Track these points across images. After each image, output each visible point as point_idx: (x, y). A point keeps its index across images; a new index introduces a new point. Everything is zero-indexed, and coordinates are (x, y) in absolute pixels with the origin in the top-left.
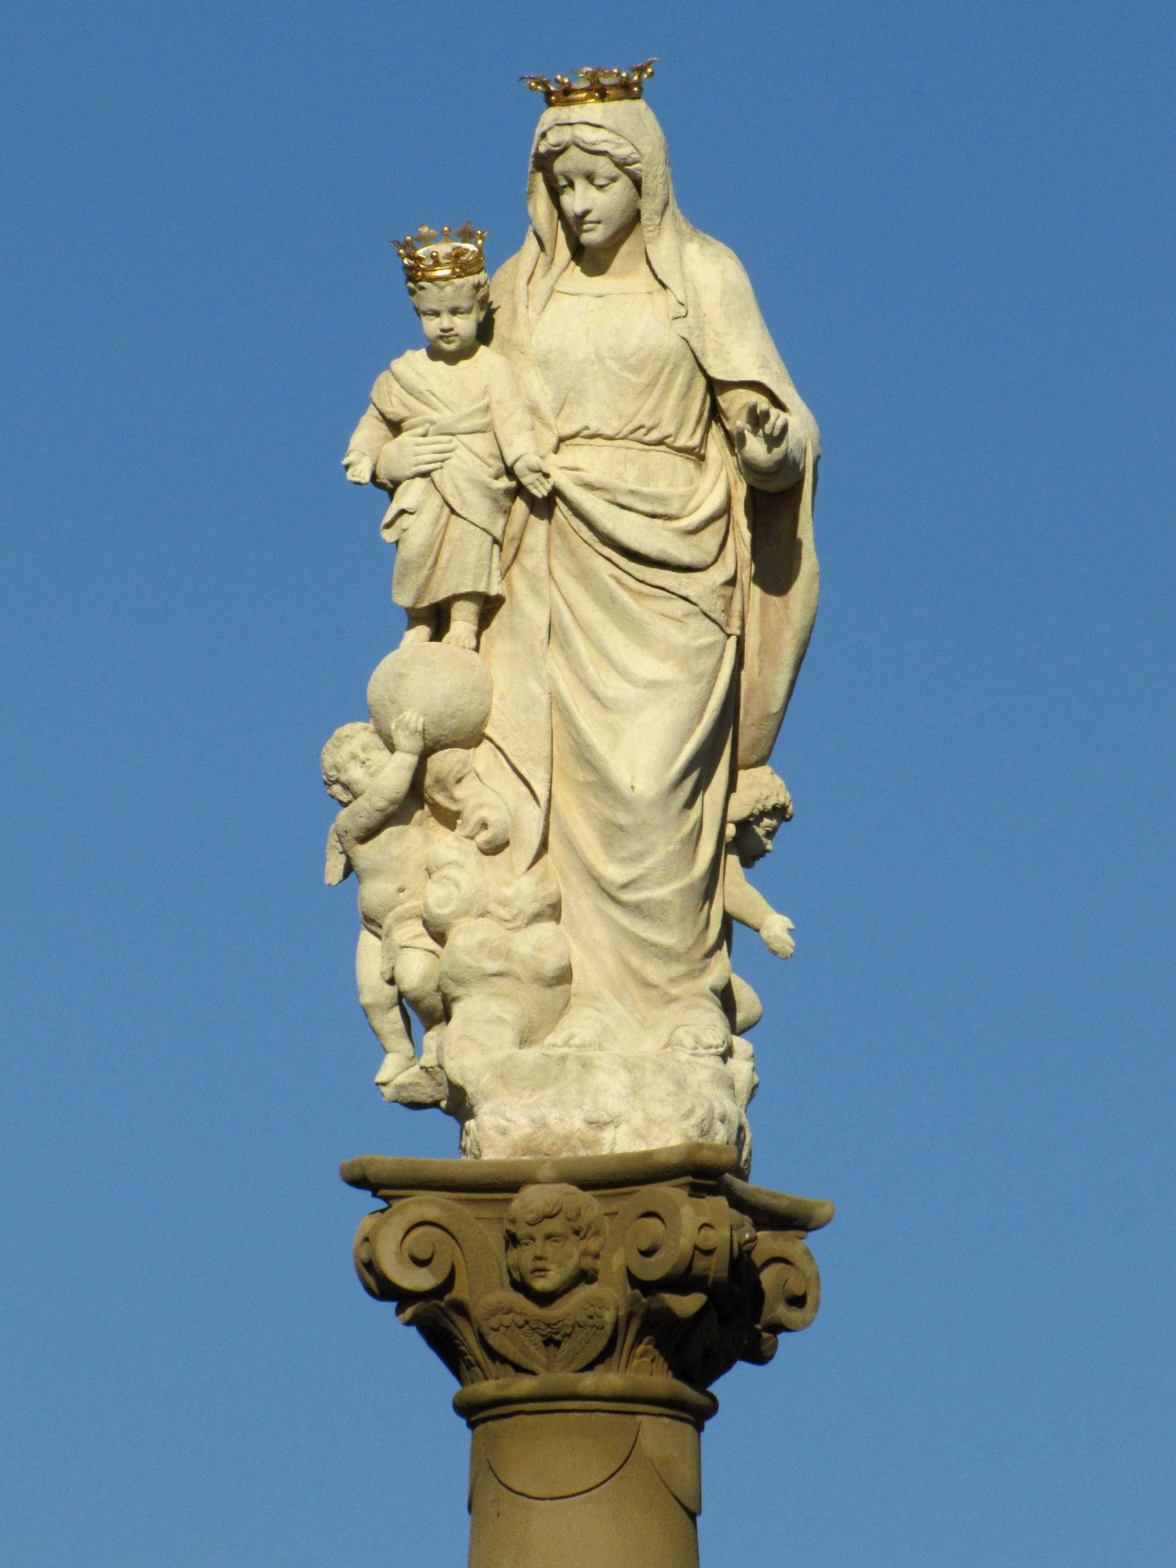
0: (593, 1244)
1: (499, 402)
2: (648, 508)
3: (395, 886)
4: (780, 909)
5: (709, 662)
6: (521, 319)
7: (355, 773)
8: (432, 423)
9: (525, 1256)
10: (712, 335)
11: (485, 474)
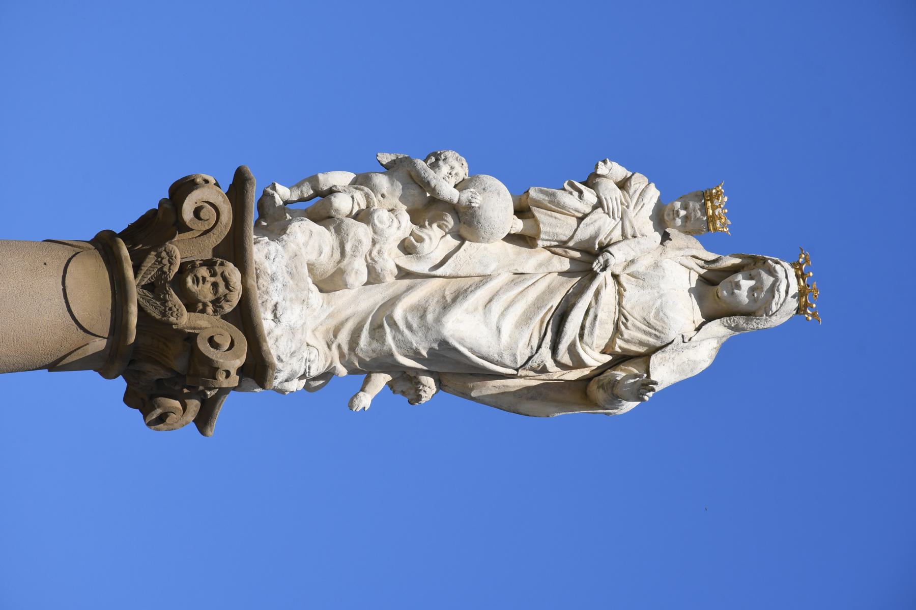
0: (210, 309)
1: (639, 242)
2: (588, 324)
3: (385, 193)
4: (374, 401)
5: (508, 360)
6: (678, 252)
7: (445, 169)
8: (628, 207)
9: (203, 272)
10: (672, 356)
11: (602, 238)
